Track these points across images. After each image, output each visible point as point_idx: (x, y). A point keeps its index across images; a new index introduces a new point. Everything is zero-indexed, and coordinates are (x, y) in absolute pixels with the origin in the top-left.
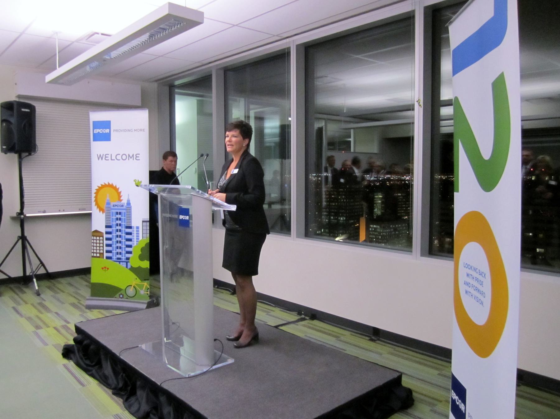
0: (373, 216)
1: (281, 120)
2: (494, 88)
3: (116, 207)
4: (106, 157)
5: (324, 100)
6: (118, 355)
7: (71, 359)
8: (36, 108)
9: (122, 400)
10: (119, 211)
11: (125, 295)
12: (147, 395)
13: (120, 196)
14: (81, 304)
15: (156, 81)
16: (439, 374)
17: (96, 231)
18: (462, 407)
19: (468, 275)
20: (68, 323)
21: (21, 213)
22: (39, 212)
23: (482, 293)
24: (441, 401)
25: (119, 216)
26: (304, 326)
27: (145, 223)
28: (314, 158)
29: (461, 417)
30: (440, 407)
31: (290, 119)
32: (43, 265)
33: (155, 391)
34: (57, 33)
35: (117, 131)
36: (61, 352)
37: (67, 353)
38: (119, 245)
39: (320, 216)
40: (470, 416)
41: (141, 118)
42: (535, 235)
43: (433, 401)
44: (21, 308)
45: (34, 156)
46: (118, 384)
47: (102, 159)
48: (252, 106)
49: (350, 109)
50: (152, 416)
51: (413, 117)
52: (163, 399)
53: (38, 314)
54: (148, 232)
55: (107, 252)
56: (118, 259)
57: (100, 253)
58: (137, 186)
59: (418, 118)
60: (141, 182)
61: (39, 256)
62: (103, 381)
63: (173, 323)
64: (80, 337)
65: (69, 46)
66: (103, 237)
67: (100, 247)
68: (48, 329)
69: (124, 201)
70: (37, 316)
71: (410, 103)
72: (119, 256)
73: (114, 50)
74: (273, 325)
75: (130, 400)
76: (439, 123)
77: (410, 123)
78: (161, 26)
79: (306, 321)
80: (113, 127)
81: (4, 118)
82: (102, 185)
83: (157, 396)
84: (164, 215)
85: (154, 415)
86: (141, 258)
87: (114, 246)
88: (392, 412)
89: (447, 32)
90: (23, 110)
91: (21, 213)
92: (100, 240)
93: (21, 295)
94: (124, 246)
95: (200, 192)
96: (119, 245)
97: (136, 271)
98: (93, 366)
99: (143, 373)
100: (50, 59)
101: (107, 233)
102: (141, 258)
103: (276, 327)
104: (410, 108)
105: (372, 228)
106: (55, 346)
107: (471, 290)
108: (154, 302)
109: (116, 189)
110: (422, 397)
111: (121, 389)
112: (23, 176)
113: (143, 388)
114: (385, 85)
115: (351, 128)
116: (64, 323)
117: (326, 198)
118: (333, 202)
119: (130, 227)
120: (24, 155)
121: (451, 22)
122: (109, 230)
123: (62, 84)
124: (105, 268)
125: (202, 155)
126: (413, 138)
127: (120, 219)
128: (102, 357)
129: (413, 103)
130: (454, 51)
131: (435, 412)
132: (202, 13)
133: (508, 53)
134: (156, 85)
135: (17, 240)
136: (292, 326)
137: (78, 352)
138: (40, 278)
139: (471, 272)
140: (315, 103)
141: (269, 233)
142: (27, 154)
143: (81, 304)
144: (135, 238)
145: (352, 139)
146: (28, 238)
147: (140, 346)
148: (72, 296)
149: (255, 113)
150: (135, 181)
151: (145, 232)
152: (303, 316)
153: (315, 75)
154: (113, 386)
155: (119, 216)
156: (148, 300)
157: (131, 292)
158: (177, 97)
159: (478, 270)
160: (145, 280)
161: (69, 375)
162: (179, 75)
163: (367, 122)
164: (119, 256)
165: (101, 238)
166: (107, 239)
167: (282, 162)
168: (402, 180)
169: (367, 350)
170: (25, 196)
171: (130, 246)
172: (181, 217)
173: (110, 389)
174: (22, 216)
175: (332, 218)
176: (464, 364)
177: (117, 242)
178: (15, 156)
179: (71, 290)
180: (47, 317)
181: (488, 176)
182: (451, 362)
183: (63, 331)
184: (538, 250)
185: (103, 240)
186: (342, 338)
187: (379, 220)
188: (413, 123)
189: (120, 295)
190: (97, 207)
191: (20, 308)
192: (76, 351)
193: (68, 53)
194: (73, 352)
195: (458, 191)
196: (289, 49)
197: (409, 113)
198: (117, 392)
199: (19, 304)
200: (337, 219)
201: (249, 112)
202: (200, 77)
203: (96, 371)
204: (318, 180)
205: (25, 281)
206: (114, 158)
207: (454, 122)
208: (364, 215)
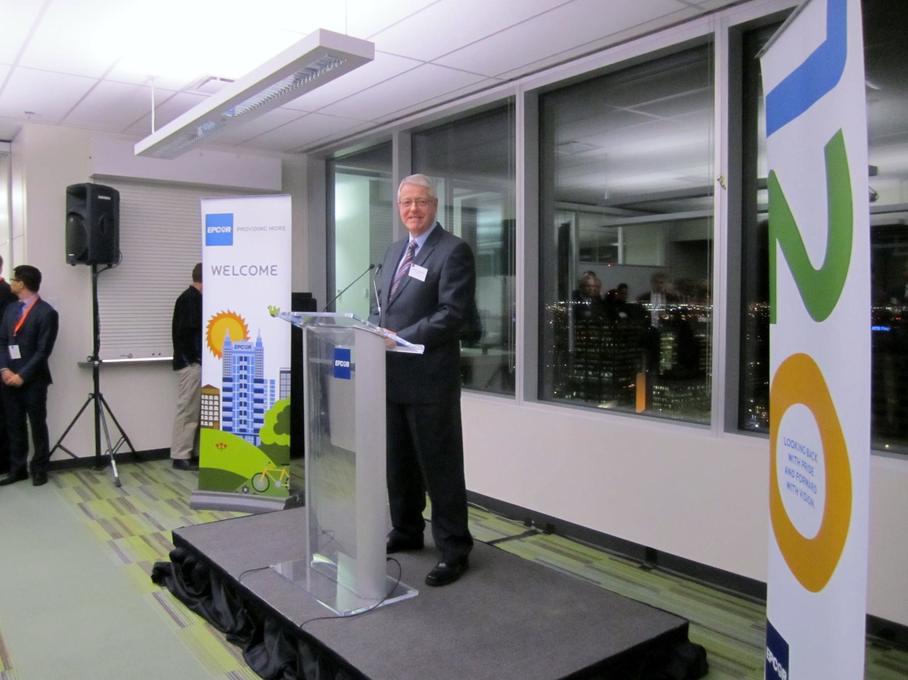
0: (658, 371)
1: (505, 212)
3: (240, 349)
5: (570, 180)
6: (237, 579)
7: (165, 585)
8: (121, 194)
9: (241, 650)
10: (244, 355)
11: (251, 487)
12: (280, 643)
13: (246, 332)
14: (184, 502)
15: (306, 152)
19: (790, 458)
20: (163, 529)
21: (95, 357)
22: (123, 356)
23: (812, 487)
25: (244, 363)
26: (534, 543)
27: (284, 375)
32: (127, 439)
33: (293, 636)
34: (153, 79)
35: (242, 229)
36: (151, 573)
37: (160, 575)
38: (243, 409)
41: (278, 211)
45: (116, 269)
46: (236, 626)
47: (219, 273)
48: (456, 191)
49: (615, 195)
50: (286, 676)
51: (712, 207)
52: (304, 649)
53: (118, 515)
54: (289, 388)
55: (225, 419)
56: (242, 430)
57: (214, 422)
58: (273, 316)
60: (279, 309)
63: (324, 532)
64: (180, 551)
65: (167, 100)
66: (219, 395)
68: (131, 539)
69: (253, 340)
70: (116, 519)
71: (706, 184)
72: (243, 426)
73: (238, 104)
74: (486, 540)
77: (705, 218)
78: (309, 66)
79: (538, 536)
80: (236, 223)
81: (71, 210)
83: (296, 647)
84: (311, 359)
85: (290, 674)
86: (278, 430)
87: (236, 410)
90: (100, 197)
91: (95, 357)
94: (250, 411)
95: (368, 323)
96: (243, 409)
97: (269, 450)
98: (198, 597)
99: (273, 607)
100: (141, 118)
101: (225, 389)
102: (278, 430)
103: (490, 544)
104: (708, 192)
105: (657, 391)
106: (142, 565)
107: (795, 481)
108: (296, 500)
109: (240, 320)
110: (719, 660)
111: (240, 633)
112: (99, 300)
113: (274, 632)
114: (669, 154)
115: (618, 226)
116: (157, 530)
119: (261, 381)
120: (100, 267)
121: (763, 52)
122: (229, 385)
124: (221, 444)
126: (711, 242)
127: (246, 368)
128: (213, 582)
129: (711, 184)
132: (371, 46)
133: (850, 102)
136: (515, 542)
137: (177, 575)
138: (122, 459)
139: (794, 452)
142: (106, 266)
143: (184, 502)
144: (269, 397)
146: (105, 397)
148: (169, 488)
149: (463, 201)
150: (270, 307)
151: (283, 388)
152: (533, 528)
153: (556, 141)
154: (228, 628)
155: (244, 363)
156: (287, 497)
157: (261, 483)
158: (338, 176)
159: (805, 450)
160: (283, 465)
162: (339, 143)
163: (642, 215)
164: (243, 426)
165: (216, 398)
166: (226, 399)
167: (505, 281)
169: (634, 583)
170: (101, 331)
171: (261, 411)
172: (338, 363)
173: (223, 632)
174: (96, 363)
176: (786, 607)
177: (241, 404)
178: (89, 268)
180: (128, 518)
181: (820, 297)
182: (765, 605)
183: (154, 542)
185: (219, 401)
186: (596, 563)
187: (667, 378)
188: (712, 217)
190: (211, 349)
191: (90, 505)
192: (173, 573)
193: (168, 109)
194: (169, 574)
195: (775, 323)
198: (234, 637)
199: (89, 499)
200: (599, 376)
201: (451, 201)
202: (375, 143)
203: (203, 604)
205: (99, 462)
208: (644, 369)
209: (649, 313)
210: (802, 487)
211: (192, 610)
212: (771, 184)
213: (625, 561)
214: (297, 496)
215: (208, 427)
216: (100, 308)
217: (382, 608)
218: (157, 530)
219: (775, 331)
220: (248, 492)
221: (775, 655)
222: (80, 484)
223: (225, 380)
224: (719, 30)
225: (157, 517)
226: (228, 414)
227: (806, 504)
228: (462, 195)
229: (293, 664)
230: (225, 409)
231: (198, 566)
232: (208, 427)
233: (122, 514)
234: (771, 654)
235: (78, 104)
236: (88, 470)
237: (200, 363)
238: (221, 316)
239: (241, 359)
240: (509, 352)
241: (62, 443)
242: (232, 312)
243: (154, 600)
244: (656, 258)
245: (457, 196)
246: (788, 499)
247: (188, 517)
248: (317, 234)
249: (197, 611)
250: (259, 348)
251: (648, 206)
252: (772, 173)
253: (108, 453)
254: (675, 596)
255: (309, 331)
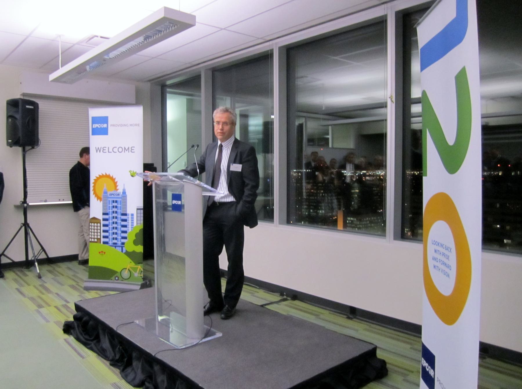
1: (265, 117)
2: (460, 85)
3: (113, 196)
4: (104, 150)
5: (305, 99)
6: (115, 329)
7: (71, 334)
8: (39, 105)
10: (115, 199)
12: (142, 365)
15: (150, 81)
16: (411, 348)
17: (94, 218)
18: (431, 372)
19: (435, 251)
21: (25, 202)
22: (41, 201)
23: (448, 267)
24: (412, 372)
25: (115, 204)
27: (139, 211)
28: (294, 158)
29: (430, 381)
30: (412, 377)
31: (272, 117)
33: (150, 361)
34: (60, 36)
35: (114, 125)
36: (62, 328)
37: (68, 328)
38: (115, 231)
39: (300, 209)
40: (439, 380)
41: (135, 115)
42: (502, 227)
43: (405, 372)
44: (24, 289)
45: (37, 149)
46: (115, 356)
47: (100, 151)
48: (237, 105)
49: (328, 108)
51: (386, 115)
52: (157, 368)
53: (40, 295)
54: (142, 218)
55: (104, 237)
57: (97, 239)
58: (132, 176)
59: (390, 114)
61: (41, 243)
62: (101, 353)
63: (166, 301)
64: (80, 314)
65: (69, 48)
66: (100, 223)
67: (97, 229)
69: (120, 191)
70: (39, 297)
72: (115, 241)
75: (126, 370)
76: (410, 120)
77: (383, 120)
78: (157, 29)
81: (10, 114)
82: (99, 175)
83: (151, 367)
84: (158, 200)
85: (149, 383)
87: (111, 232)
88: (368, 381)
89: (416, 35)
90: (27, 107)
91: (25, 202)
92: (97, 226)
93: (23, 277)
94: (119, 232)
96: (115, 231)
97: (131, 255)
98: (92, 341)
101: (104, 220)
102: (135, 243)
103: (262, 306)
104: (383, 105)
106: (57, 323)
108: (147, 283)
109: (113, 179)
111: (117, 361)
112: (27, 168)
113: (138, 359)
114: (359, 84)
115: (329, 125)
116: (64, 303)
117: (307, 193)
118: (312, 196)
119: (125, 215)
120: (27, 148)
121: (419, 24)
122: (106, 217)
123: (65, 82)
124: (102, 252)
125: (193, 146)
126: (386, 134)
127: (116, 207)
128: (101, 332)
130: (421, 50)
131: (407, 381)
132: (194, 17)
133: (469, 52)
134: (149, 84)
135: (20, 227)
136: (275, 305)
138: (41, 262)
140: (296, 101)
141: (253, 224)
142: (30, 147)
144: (130, 224)
145: (330, 137)
146: (30, 225)
147: (135, 321)
149: (240, 111)
150: (130, 171)
151: (139, 218)
152: (285, 297)
153: (296, 76)
154: (111, 358)
155: (115, 204)
156: (141, 282)
157: (126, 274)
158: (168, 96)
159: (444, 246)
160: (139, 263)
161: (70, 348)
162: (170, 76)
164: (115, 241)
165: (99, 225)
166: (104, 225)
167: (265, 156)
168: (377, 176)
170: (28, 186)
171: (125, 232)
173: (108, 360)
174: (25, 205)
175: (312, 211)
178: (20, 149)
179: (70, 273)
181: (452, 160)
182: (421, 338)
183: (64, 310)
184: (505, 241)
185: (100, 226)
187: (356, 213)
188: (386, 120)
189: (115, 278)
191: (23, 289)
192: (76, 327)
193: (69, 54)
194: (74, 328)
195: (426, 176)
196: (272, 50)
197: (382, 111)
198: (114, 363)
199: (22, 286)
200: (317, 212)
203: (95, 344)
204: (298, 176)
205: (28, 264)
206: (111, 150)
207: (423, 119)
209: (345, 177)
210: (443, 267)
211: (88, 348)
212: (423, 100)
213: (338, 314)
214: (147, 281)
215: (94, 242)
216: (27, 173)
217: (201, 344)
218: (64, 303)
219: (426, 181)
220: (118, 279)
221: (427, 362)
222: (17, 277)
223: (104, 214)
224: (389, 13)
225: (64, 296)
226: (106, 234)
227: (445, 276)
228: (242, 107)
229: (151, 377)
230: (104, 231)
231: (91, 323)
232: (94, 242)
233: (43, 294)
234: (425, 361)
235: (13, 52)
236: (20, 269)
237: (89, 206)
238: (101, 177)
239: (113, 202)
240: (270, 198)
241: (5, 253)
242: (108, 174)
243: (65, 343)
244: (350, 144)
245: (237, 108)
246: (435, 275)
247: (82, 295)
248: (157, 130)
249: (91, 349)
250: (124, 195)
251: (344, 114)
252: (424, 93)
253: (33, 259)
254: (367, 333)
255: (156, 184)
